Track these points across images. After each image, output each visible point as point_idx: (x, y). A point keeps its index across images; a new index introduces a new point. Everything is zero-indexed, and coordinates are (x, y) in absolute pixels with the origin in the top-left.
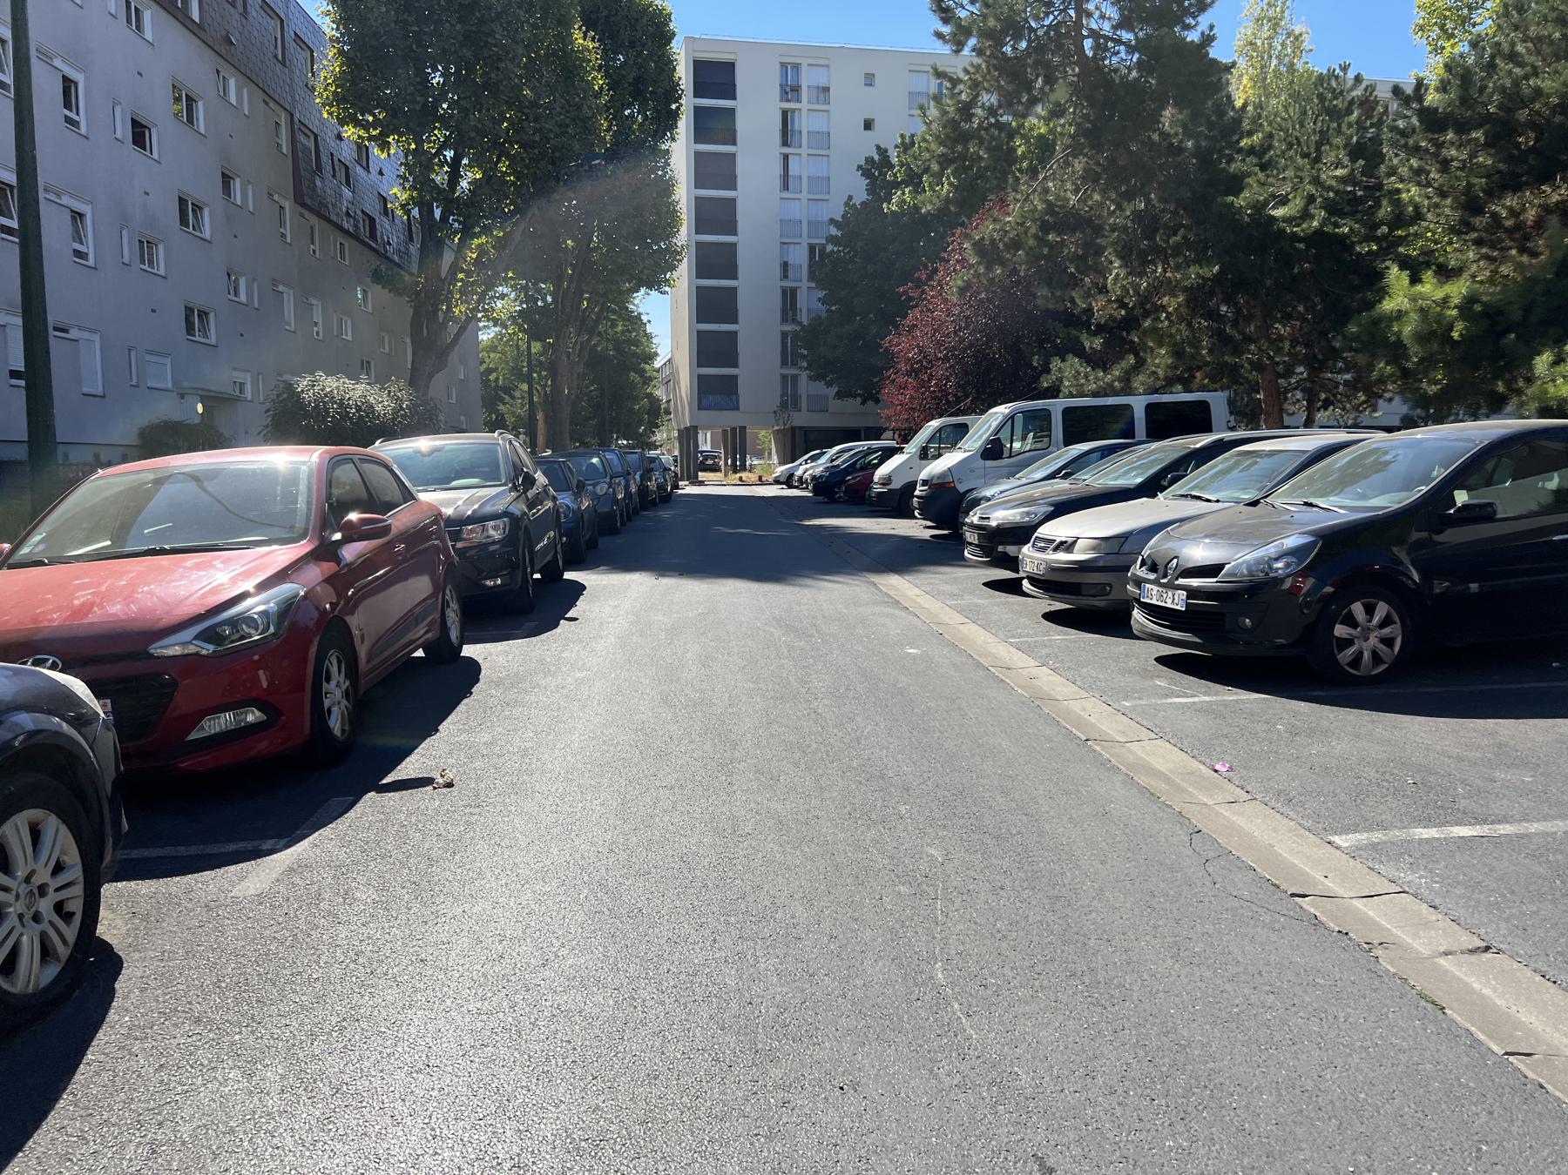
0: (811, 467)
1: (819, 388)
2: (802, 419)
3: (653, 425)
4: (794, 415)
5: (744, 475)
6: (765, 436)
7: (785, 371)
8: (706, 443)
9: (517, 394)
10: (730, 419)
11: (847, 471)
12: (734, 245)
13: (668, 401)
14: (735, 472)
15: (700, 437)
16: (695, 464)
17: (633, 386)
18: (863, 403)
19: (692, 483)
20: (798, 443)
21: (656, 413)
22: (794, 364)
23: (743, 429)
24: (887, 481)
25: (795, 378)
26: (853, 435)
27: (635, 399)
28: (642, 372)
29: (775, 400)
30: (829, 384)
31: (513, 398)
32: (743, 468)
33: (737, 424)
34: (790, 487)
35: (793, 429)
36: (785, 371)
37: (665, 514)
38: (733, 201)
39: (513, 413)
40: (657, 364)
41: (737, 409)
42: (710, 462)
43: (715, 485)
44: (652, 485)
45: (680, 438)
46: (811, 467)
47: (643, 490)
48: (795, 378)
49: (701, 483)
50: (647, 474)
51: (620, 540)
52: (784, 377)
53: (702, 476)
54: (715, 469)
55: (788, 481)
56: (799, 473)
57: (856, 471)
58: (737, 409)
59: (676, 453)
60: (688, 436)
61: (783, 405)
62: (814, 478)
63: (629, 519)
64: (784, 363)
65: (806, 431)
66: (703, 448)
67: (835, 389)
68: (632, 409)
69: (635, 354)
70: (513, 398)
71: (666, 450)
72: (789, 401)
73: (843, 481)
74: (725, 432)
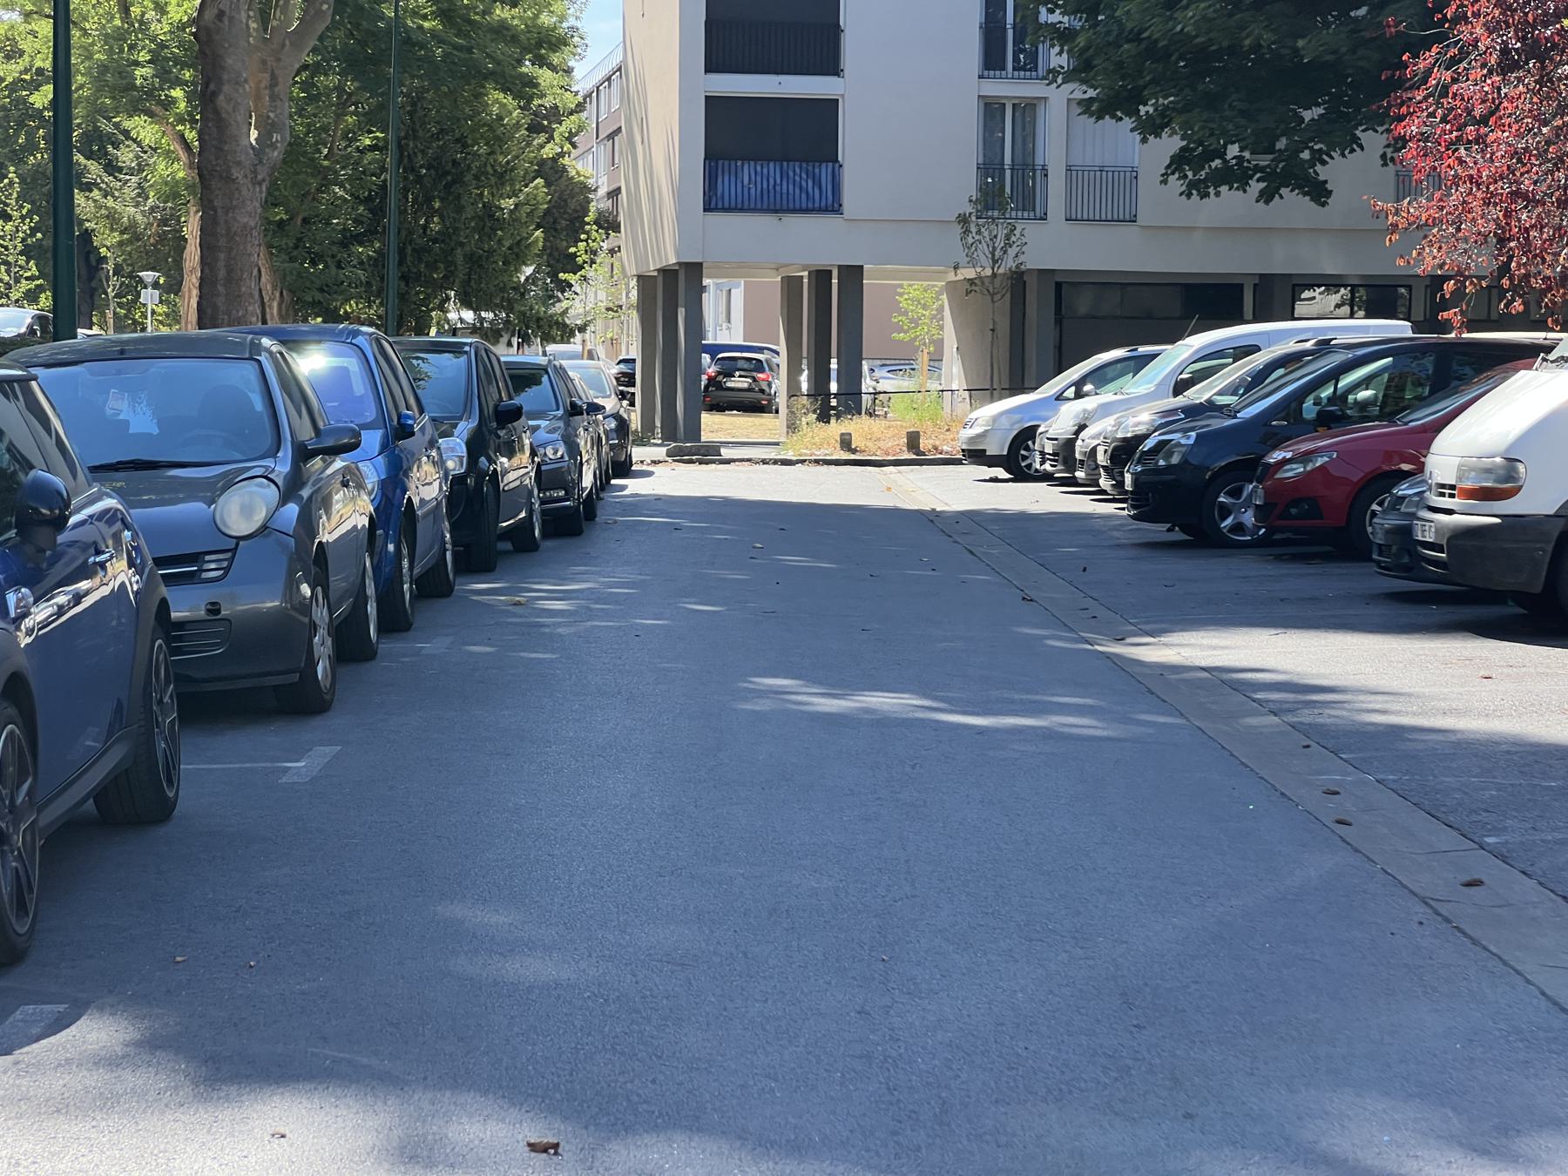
0: (1122, 402)
1: (1117, 141)
2: (1054, 244)
3: (561, 263)
4: (1030, 231)
5: (857, 427)
6: (921, 308)
7: (999, 88)
8: (730, 316)
9: (126, 156)
10: (809, 241)
11: (1267, 431)
12: (830, 106)
13: (614, 194)
14: (824, 417)
15: (711, 304)
16: (692, 388)
17: (497, 135)
18: (1267, 196)
19: (678, 455)
20: (1045, 324)
21: (569, 220)
22: (1028, 65)
23: (852, 274)
24: (1499, 483)
25: (1027, 110)
26: (1213, 301)
27: (503, 178)
28: (524, 89)
29: (963, 185)
30: (1150, 128)
31: (112, 168)
32: (851, 402)
33: (832, 258)
34: (1021, 474)
35: (1018, 280)
36: (999, 88)
37: (554, 593)
38: (827, 109)
39: (112, 218)
40: (586, 70)
41: (834, 207)
42: (738, 382)
43: (766, 464)
44: (515, 471)
45: (645, 307)
46: (1122, 402)
47: (472, 496)
48: (1027, 110)
49: (708, 454)
50: (497, 427)
51: (302, 759)
52: (992, 110)
53: (713, 426)
54: (756, 404)
55: (1016, 460)
56: (1059, 424)
57: (1331, 418)
58: (834, 207)
59: (635, 352)
60: (671, 293)
61: (991, 199)
62: (1124, 451)
63: (395, 621)
64: (992, 60)
65: (1061, 286)
66: (716, 334)
67: (1170, 143)
68: (490, 211)
69: (502, 31)
70: (112, 168)
71: (597, 342)
72: (1006, 187)
73: (1251, 468)
74: (791, 286)
